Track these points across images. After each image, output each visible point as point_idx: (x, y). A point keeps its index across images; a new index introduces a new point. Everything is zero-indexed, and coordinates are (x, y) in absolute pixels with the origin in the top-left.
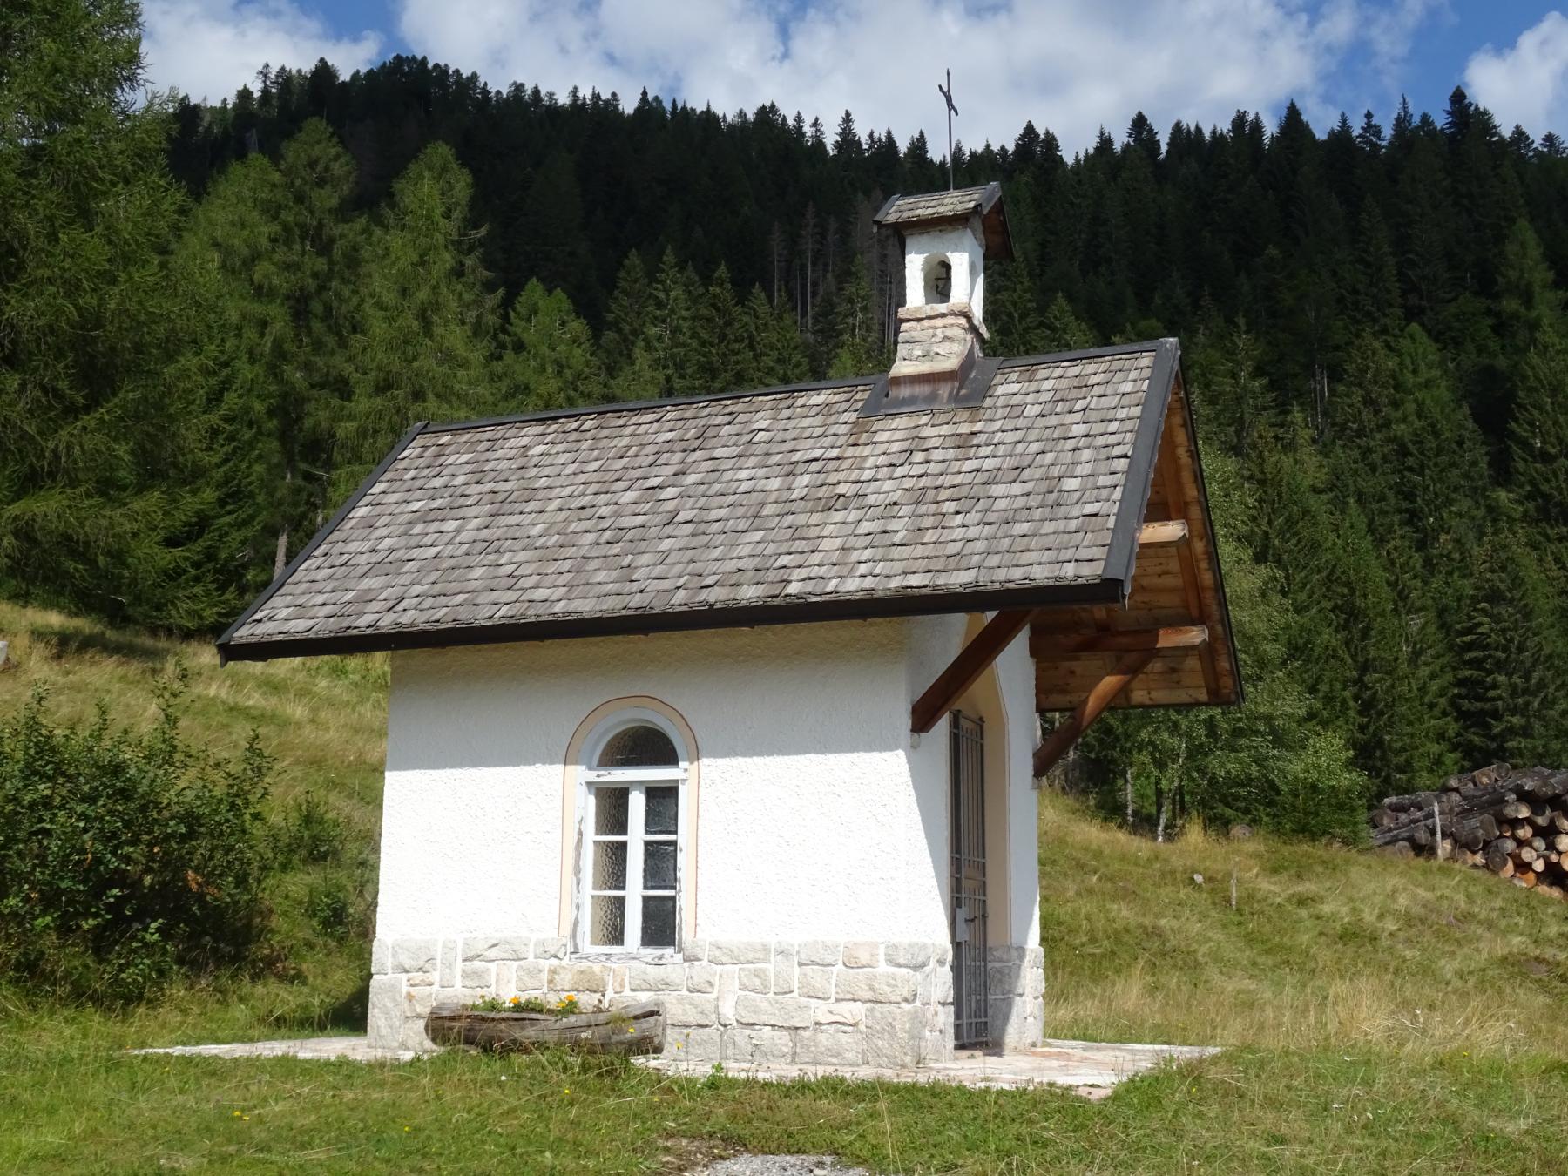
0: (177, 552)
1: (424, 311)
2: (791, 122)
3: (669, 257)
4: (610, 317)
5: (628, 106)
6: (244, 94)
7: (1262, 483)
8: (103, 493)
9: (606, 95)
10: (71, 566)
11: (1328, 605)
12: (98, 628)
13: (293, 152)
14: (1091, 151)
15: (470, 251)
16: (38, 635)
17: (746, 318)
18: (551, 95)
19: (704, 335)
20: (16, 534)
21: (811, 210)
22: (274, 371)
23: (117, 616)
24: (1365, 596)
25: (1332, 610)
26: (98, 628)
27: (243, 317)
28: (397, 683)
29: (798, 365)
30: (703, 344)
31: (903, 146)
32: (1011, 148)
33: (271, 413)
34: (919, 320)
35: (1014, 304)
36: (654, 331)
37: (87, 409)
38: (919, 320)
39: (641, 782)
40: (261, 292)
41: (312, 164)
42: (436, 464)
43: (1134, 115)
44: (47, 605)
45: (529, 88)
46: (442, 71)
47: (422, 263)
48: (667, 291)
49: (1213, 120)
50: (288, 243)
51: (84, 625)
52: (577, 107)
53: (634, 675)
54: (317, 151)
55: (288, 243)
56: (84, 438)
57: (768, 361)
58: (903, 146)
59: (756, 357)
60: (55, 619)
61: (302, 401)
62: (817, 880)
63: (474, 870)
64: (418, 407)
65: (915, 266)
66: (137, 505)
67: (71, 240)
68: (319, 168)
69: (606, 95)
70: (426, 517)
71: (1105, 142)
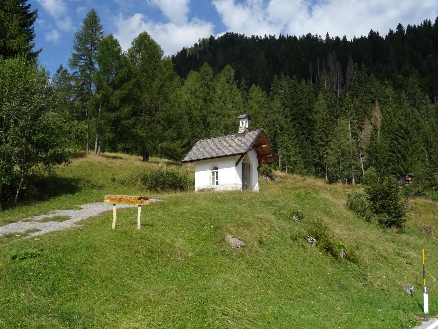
0: (184, 149)
1: (224, 101)
2: (315, 36)
3: (283, 75)
4: (271, 89)
5: (277, 37)
6: (196, 45)
7: (406, 116)
8: (172, 141)
9: (272, 35)
10: (168, 152)
11: (422, 141)
12: (173, 161)
13: (202, 70)
14: (388, 34)
16: (165, 163)
17: (300, 86)
18: (260, 37)
19: (291, 91)
20: (161, 148)
21: (318, 58)
22: (201, 112)
23: (176, 160)
24: (430, 138)
25: (423, 142)
26: (173, 161)
28: (196, 164)
29: (312, 96)
30: (291, 93)
31: (341, 39)
32: (367, 36)
33: (201, 120)
35: (363, 76)
36: (280, 91)
37: (169, 129)
40: (197, 97)
41: (205, 71)
42: (200, 144)
43: (398, 24)
44: (166, 158)
45: (256, 36)
46: (236, 34)
47: (223, 92)
48: (283, 82)
49: (418, 22)
50: (202, 87)
51: (171, 161)
52: (266, 38)
53: (214, 161)
54: (206, 69)
55: (202, 87)
56: (170, 133)
57: (305, 95)
58: (341, 39)
59: (303, 95)
60: (166, 160)
61: (206, 117)
62: (229, 178)
63: (203, 179)
64: (223, 119)
66: (177, 143)
68: (207, 72)
69: (272, 35)
70: (198, 149)
71: (391, 32)
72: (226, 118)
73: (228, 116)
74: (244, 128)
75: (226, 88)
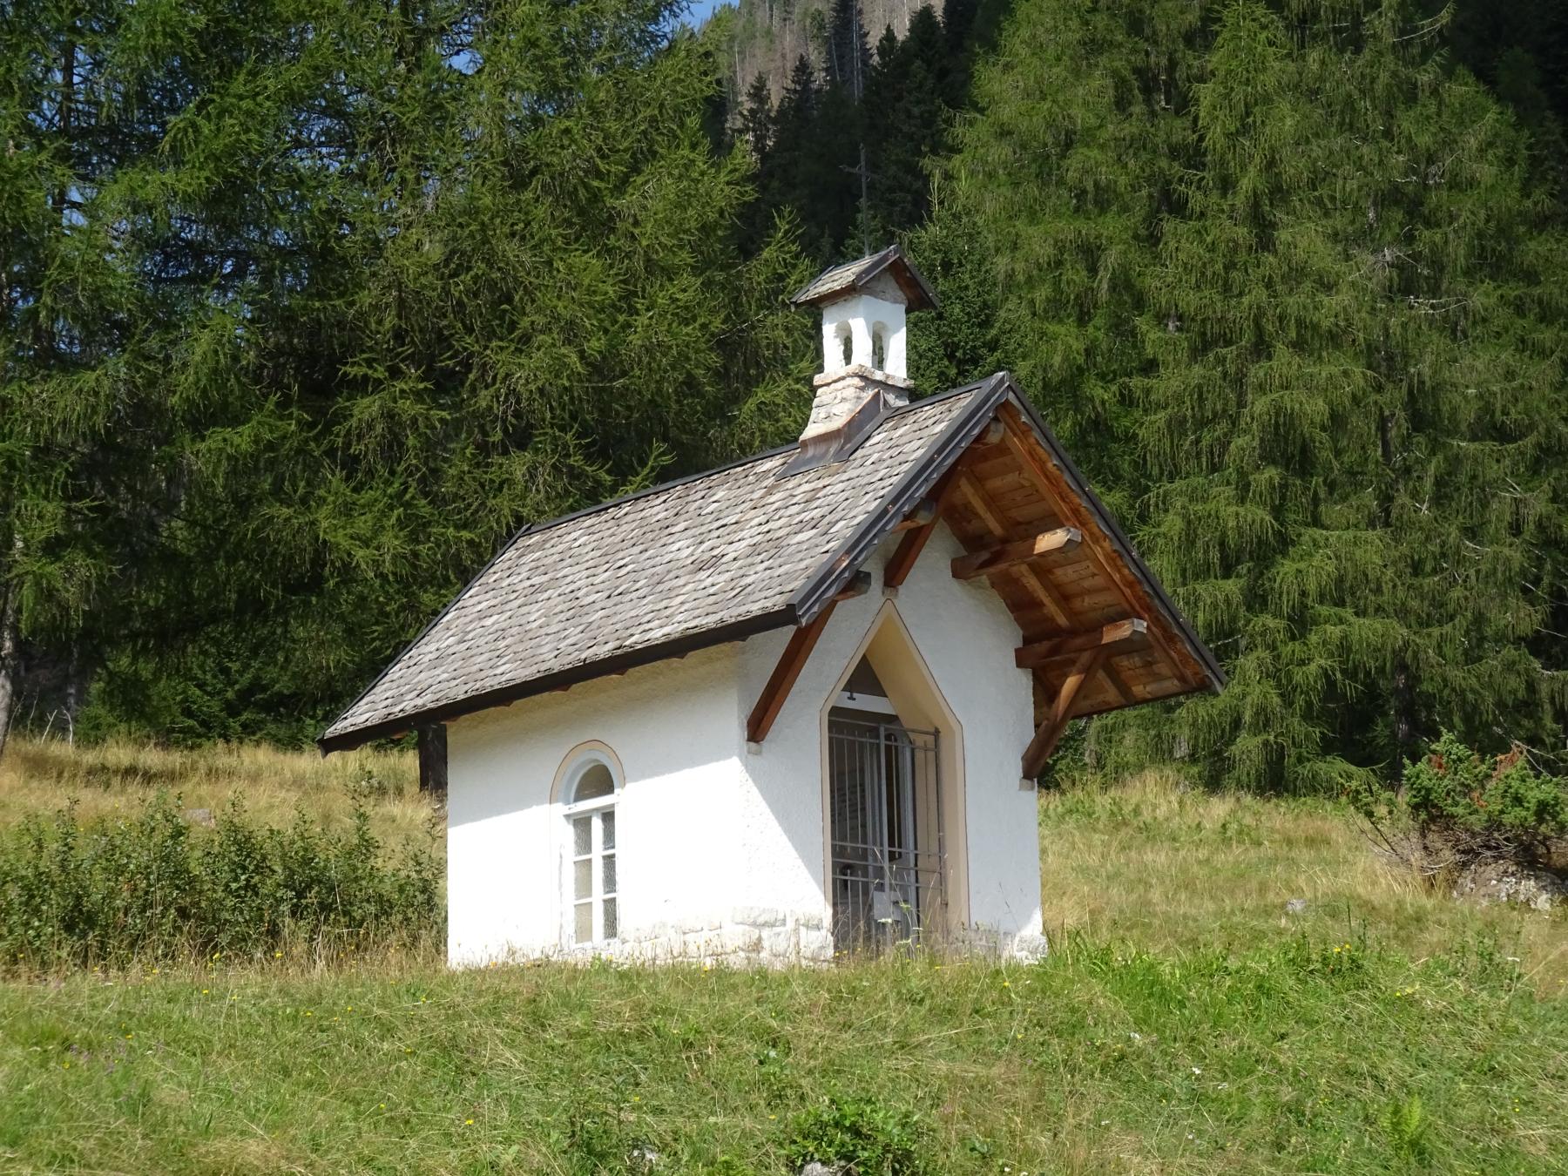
15: (1426, 53)
27: (1060, 247)
34: (828, 384)
38: (828, 384)
39: (597, 810)
47: (1244, 130)
62: (711, 856)
63: (508, 880)
64: (1256, 372)
65: (829, 330)
67: (570, 268)
72: (1284, 360)
73: (1299, 346)
74: (850, 388)
75: (1268, 80)
